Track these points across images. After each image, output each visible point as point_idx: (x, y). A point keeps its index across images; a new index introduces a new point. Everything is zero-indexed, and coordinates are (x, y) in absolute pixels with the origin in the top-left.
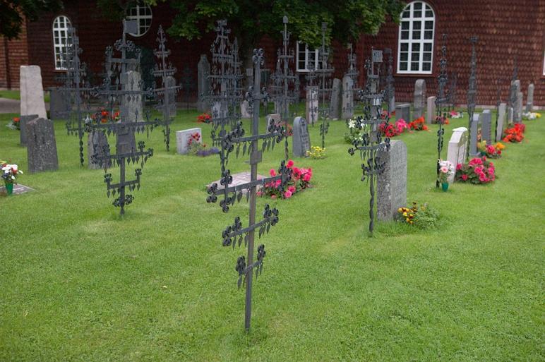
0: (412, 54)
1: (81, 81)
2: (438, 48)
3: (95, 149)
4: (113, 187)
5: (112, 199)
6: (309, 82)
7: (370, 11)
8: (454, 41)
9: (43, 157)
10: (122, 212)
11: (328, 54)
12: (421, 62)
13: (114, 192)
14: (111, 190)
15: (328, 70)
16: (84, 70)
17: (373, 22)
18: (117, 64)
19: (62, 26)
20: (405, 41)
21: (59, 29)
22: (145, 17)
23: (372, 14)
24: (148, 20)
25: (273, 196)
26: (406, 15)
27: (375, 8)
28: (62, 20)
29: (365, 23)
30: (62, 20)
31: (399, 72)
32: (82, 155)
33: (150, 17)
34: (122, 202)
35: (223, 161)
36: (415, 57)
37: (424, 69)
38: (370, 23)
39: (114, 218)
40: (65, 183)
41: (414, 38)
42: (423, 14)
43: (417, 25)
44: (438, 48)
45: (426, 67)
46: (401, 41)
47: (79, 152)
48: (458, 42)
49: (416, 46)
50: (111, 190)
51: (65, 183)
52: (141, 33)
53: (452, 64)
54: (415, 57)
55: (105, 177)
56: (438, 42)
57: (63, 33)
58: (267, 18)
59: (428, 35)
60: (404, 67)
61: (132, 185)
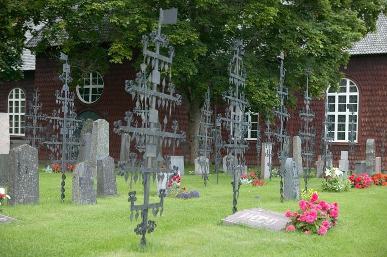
0: (339, 124)
1: (69, 111)
2: (363, 119)
3: (80, 182)
4: (137, 208)
5: (134, 224)
6: (267, 137)
7: (317, 77)
8: (378, 114)
9: (24, 188)
10: (144, 241)
11: (311, 99)
13: (137, 215)
14: (135, 212)
15: (310, 115)
16: (72, 100)
17: (320, 87)
18: (152, 58)
19: (17, 97)
21: (14, 100)
23: (318, 80)
24: (100, 89)
25: (306, 232)
27: (320, 74)
28: (17, 91)
29: (312, 87)
30: (17, 91)
32: (63, 190)
33: (102, 86)
34: (144, 228)
35: (235, 193)
38: (317, 88)
39: (134, 248)
40: (52, 215)
42: (348, 89)
44: (363, 119)
47: (60, 187)
48: (381, 114)
49: (341, 118)
50: (135, 212)
51: (52, 215)
52: (92, 101)
53: (376, 134)
55: (129, 195)
56: (363, 115)
57: (17, 103)
58: (222, 81)
59: (353, 108)
61: (155, 209)
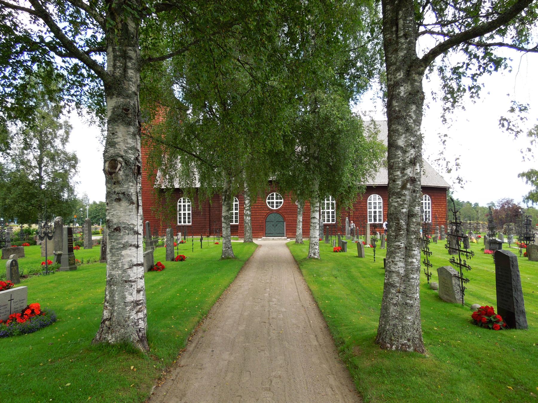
12: (187, 220)
20: (236, 211)
22: (275, 196)
26: (180, 202)
28: (426, 196)
31: (178, 224)
36: (185, 218)
37: (332, 221)
41: (329, 212)
43: (184, 206)
45: (333, 221)
46: (190, 212)
54: (185, 218)
60: (180, 222)
